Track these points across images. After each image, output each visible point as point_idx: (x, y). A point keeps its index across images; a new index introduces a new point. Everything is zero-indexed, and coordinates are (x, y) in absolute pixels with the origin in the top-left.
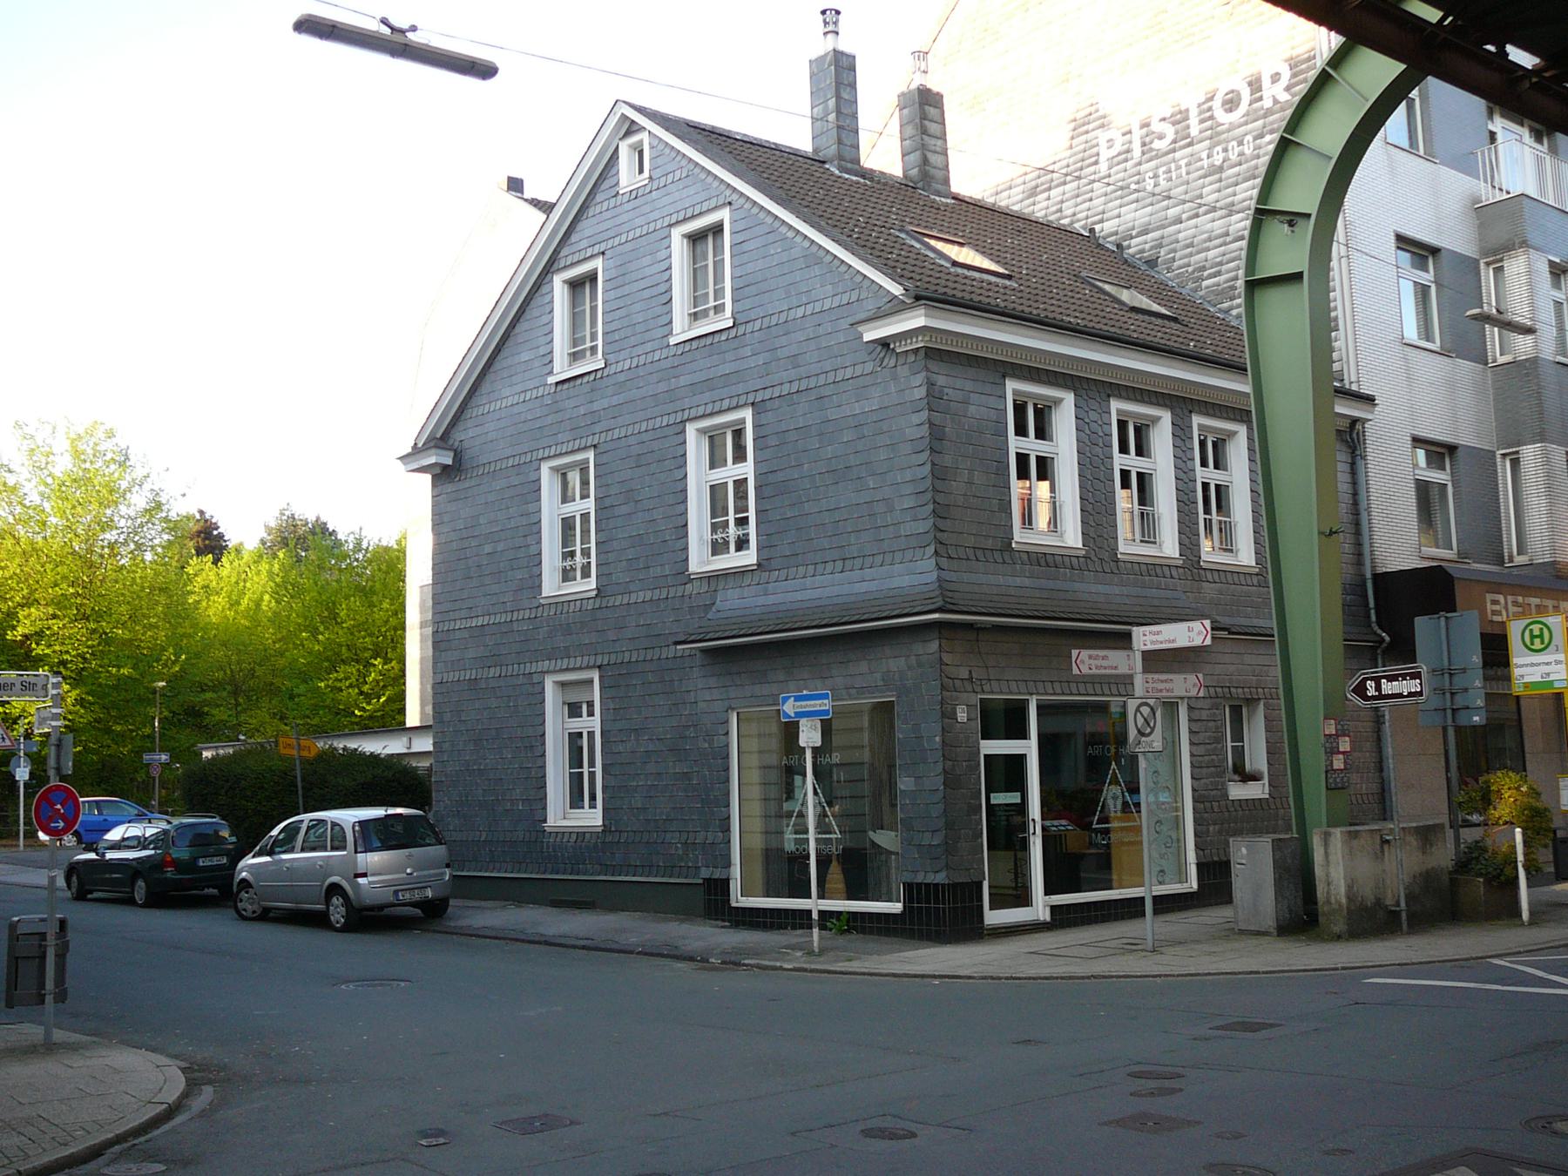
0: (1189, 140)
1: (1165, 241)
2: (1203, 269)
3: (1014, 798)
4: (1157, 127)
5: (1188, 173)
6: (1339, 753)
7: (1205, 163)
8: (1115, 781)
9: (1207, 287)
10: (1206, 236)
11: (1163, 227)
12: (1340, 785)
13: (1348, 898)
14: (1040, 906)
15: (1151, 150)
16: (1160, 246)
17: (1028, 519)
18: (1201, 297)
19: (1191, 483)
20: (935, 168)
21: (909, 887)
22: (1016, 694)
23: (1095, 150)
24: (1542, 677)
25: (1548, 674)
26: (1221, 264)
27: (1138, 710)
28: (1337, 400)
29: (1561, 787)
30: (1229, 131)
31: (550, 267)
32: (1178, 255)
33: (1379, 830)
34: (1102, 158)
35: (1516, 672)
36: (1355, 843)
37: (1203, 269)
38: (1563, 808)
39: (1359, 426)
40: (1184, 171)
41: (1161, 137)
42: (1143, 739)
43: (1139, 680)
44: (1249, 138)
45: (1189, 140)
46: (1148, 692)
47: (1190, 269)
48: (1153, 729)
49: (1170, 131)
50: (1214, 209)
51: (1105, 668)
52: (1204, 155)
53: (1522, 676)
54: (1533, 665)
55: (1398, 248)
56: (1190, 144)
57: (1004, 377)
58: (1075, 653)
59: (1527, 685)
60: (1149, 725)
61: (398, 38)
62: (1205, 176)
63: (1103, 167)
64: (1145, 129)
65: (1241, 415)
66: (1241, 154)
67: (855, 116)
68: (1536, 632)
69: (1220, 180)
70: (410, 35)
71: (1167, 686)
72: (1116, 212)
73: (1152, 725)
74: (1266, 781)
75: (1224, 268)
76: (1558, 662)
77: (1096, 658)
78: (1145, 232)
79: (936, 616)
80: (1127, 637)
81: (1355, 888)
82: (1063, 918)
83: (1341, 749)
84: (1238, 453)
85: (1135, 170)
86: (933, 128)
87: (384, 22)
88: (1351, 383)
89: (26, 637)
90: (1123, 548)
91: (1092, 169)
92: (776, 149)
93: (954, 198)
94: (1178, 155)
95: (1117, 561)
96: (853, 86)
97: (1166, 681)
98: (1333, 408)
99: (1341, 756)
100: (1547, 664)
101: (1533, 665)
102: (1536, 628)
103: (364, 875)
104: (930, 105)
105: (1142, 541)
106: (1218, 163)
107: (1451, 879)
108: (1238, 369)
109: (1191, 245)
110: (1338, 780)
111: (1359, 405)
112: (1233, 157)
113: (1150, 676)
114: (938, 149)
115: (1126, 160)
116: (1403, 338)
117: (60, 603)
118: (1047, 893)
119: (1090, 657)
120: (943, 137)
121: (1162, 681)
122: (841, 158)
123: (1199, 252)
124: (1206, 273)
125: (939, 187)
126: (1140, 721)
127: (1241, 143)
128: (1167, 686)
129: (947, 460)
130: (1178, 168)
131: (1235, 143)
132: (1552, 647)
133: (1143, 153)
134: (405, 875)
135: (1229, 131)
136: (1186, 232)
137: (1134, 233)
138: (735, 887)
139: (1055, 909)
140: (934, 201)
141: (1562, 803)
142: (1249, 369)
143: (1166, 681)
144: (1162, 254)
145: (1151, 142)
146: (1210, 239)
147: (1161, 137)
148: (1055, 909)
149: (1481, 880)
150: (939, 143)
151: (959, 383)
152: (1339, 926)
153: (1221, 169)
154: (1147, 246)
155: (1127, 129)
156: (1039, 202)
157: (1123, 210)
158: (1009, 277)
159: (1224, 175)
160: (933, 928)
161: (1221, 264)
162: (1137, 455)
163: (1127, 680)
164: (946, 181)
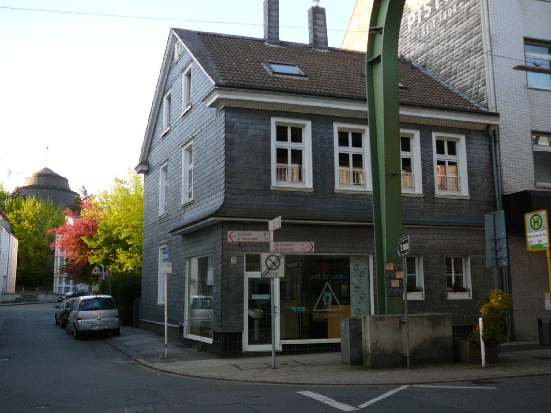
0: (435, 12)
1: (429, 57)
2: (440, 66)
3: (255, 297)
4: (426, 8)
5: (436, 26)
6: (395, 279)
7: (441, 20)
8: (327, 290)
9: (442, 74)
10: (441, 52)
11: (428, 51)
12: (396, 294)
13: (373, 349)
14: (278, 343)
15: (424, 18)
16: (427, 59)
17: (443, 186)
18: (440, 79)
19: (430, 162)
20: (321, 38)
21: (215, 333)
22: (333, 253)
23: (407, 23)
24: (539, 242)
25: (541, 241)
26: (446, 63)
27: (268, 258)
28: (401, 109)
29: (545, 298)
30: (448, 4)
31: (164, 94)
32: (433, 61)
33: (399, 317)
34: (409, 26)
35: (529, 240)
36: (379, 323)
37: (440, 66)
38: (546, 309)
39: (492, 128)
40: (434, 25)
41: (427, 12)
42: (271, 271)
43: (272, 244)
44: (455, 5)
45: (435, 12)
46: (277, 250)
47: (437, 67)
48: (278, 267)
49: (429, 9)
50: (443, 40)
51: (249, 239)
52: (440, 17)
53: (531, 242)
54: (535, 236)
55: (526, 44)
56: (436, 13)
57: (270, 117)
58: (229, 232)
59: (533, 247)
60: (275, 265)
61: (537, 67)
62: (441, 26)
63: (409, 29)
64: (422, 11)
65: (363, 121)
66: (452, 13)
67: (277, 22)
68: (536, 220)
69: (446, 26)
70: (541, 66)
71: (290, 247)
72: (413, 48)
73: (277, 265)
74: (424, 292)
75: (448, 64)
76: (544, 235)
77: (242, 235)
78: (422, 54)
79: (212, 219)
80: (267, 224)
81: (378, 344)
82: (287, 350)
83: (398, 277)
84: (366, 140)
85: (419, 29)
86: (319, 22)
87: (534, 64)
88: (492, 108)
89: (125, 238)
90: (338, 187)
91: (406, 31)
92: (243, 38)
93: (329, 49)
94: (432, 18)
95: (334, 193)
96: (277, 10)
97: (289, 245)
98: (399, 113)
99: (398, 281)
100: (540, 235)
101: (535, 236)
102: (536, 217)
103: (80, 319)
104: (318, 13)
105: (354, 184)
106: (445, 19)
107: (454, 342)
108: (361, 100)
109: (437, 57)
110: (395, 292)
111: (491, 118)
112: (450, 15)
113: (279, 243)
114: (322, 31)
115: (416, 25)
116: (527, 85)
117: (134, 227)
118: (282, 339)
119: (239, 234)
120: (325, 25)
121: (287, 245)
122: (269, 38)
123: (439, 59)
124: (442, 68)
125: (322, 46)
126: (269, 263)
127: (452, 9)
128: (290, 247)
129: (235, 153)
130: (432, 24)
131: (450, 9)
132: (542, 227)
133: (422, 20)
134: (96, 320)
135: (448, 4)
136: (435, 51)
137: (419, 55)
138: (185, 329)
139: (284, 346)
140: (317, 52)
141: (546, 306)
142: (367, 99)
143: (289, 245)
144: (428, 62)
145: (424, 15)
146: (442, 53)
147: (427, 12)
148: (284, 346)
149: (468, 343)
150: (323, 28)
151: (244, 121)
152: (368, 363)
153: (445, 22)
154: (423, 60)
155: (416, 12)
156: (472, 61)
157: (416, 46)
158: (305, 76)
159: (447, 24)
160: (308, 349)
161: (446, 63)
162: (449, 154)
163: (265, 246)
164: (326, 43)
